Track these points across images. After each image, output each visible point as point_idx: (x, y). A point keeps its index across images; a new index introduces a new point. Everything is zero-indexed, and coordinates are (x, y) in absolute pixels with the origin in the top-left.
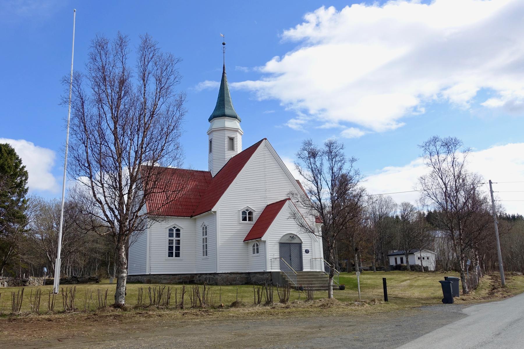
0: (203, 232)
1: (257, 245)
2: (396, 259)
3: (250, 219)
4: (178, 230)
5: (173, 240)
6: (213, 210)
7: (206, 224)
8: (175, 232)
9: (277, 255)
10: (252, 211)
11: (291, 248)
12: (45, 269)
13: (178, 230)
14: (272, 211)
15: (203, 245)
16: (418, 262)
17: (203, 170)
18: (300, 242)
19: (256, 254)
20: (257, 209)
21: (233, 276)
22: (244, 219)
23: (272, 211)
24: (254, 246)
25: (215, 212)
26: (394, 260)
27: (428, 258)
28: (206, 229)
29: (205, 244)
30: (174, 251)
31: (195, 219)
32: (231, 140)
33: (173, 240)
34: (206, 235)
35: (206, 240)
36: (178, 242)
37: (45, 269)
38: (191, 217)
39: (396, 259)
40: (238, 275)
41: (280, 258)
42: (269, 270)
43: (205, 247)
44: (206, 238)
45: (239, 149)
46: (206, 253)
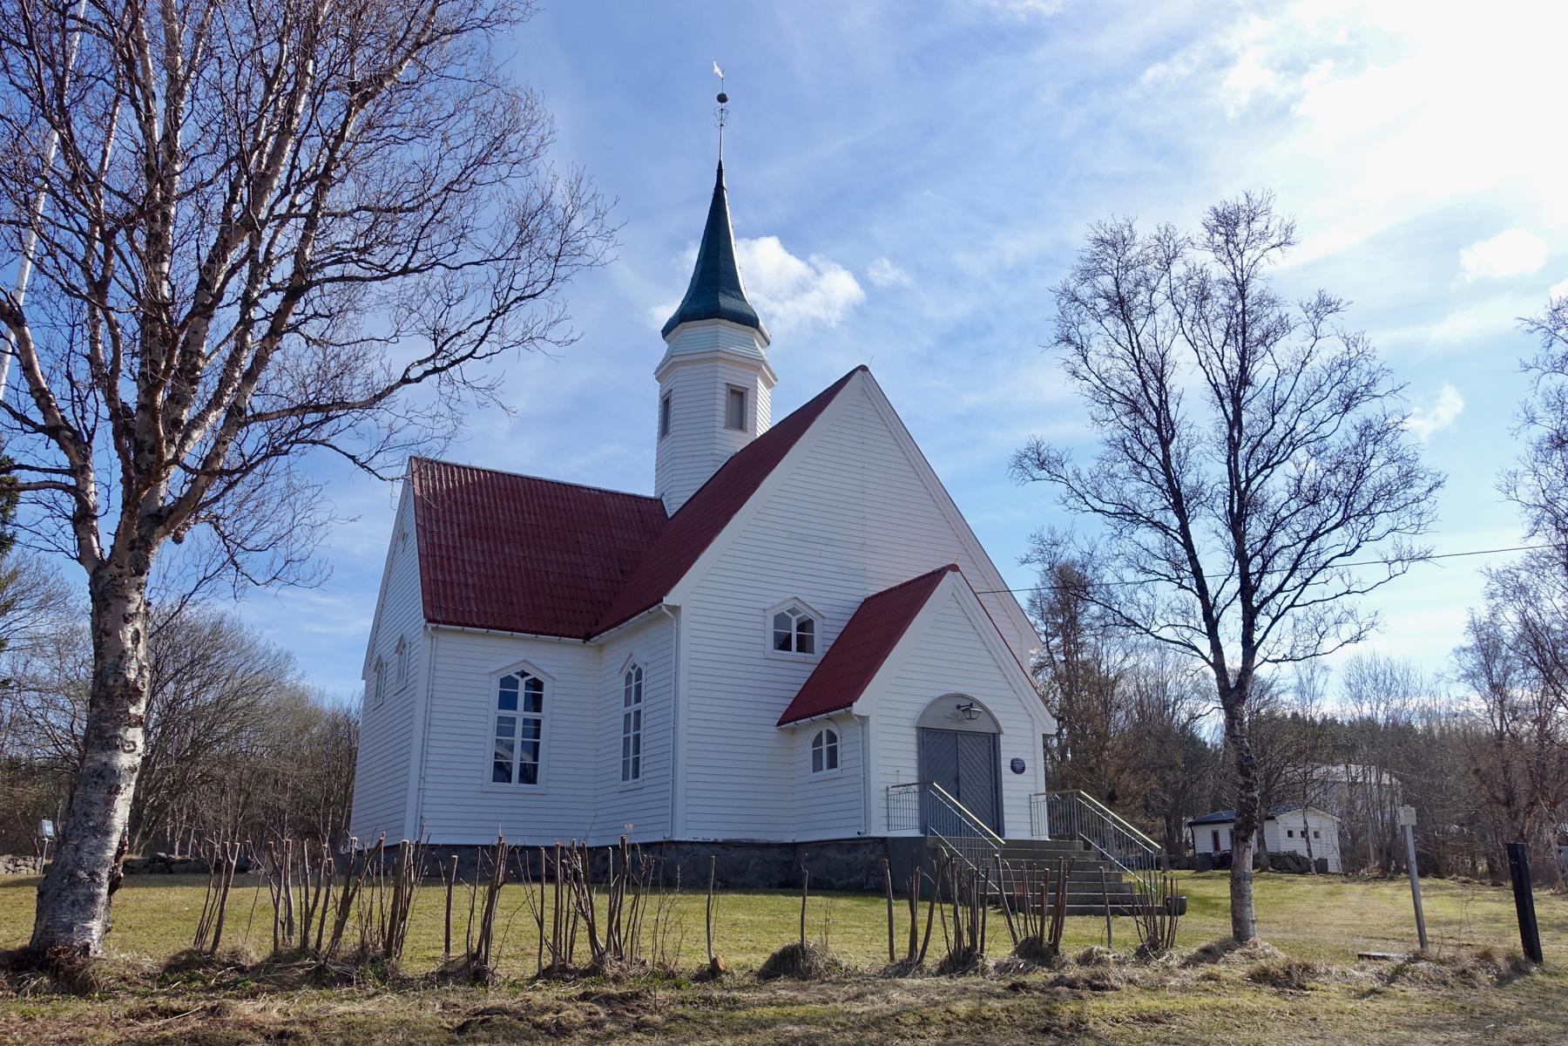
0: (628, 692)
1: (832, 737)
2: (1215, 835)
3: (804, 645)
4: (536, 685)
5: (513, 720)
6: (668, 600)
7: (641, 659)
8: (521, 691)
9: (910, 773)
10: (812, 616)
11: (957, 750)
12: (48, 828)
13: (536, 685)
14: (885, 617)
15: (626, 740)
16: (1287, 846)
17: (638, 493)
18: (994, 730)
19: (826, 772)
20: (833, 602)
21: (735, 854)
22: (783, 643)
23: (885, 617)
24: (818, 741)
25: (675, 609)
26: (1210, 840)
27: (1290, 834)
28: (639, 677)
29: (632, 734)
30: (517, 767)
31: (601, 647)
32: (736, 398)
33: (513, 720)
34: (638, 700)
35: (625, 770)
36: (535, 728)
37: (48, 828)
38: (587, 637)
39: (1215, 835)
40: (753, 852)
41: (924, 784)
42: (878, 831)
43: (633, 746)
44: (638, 713)
45: (764, 419)
46: (633, 769)
